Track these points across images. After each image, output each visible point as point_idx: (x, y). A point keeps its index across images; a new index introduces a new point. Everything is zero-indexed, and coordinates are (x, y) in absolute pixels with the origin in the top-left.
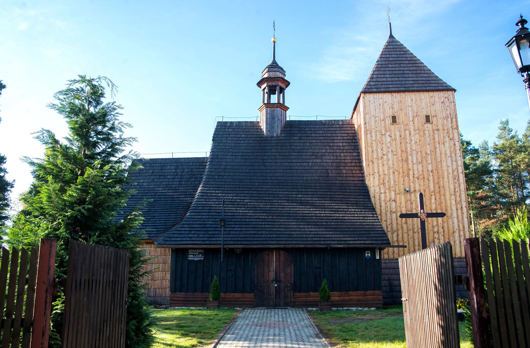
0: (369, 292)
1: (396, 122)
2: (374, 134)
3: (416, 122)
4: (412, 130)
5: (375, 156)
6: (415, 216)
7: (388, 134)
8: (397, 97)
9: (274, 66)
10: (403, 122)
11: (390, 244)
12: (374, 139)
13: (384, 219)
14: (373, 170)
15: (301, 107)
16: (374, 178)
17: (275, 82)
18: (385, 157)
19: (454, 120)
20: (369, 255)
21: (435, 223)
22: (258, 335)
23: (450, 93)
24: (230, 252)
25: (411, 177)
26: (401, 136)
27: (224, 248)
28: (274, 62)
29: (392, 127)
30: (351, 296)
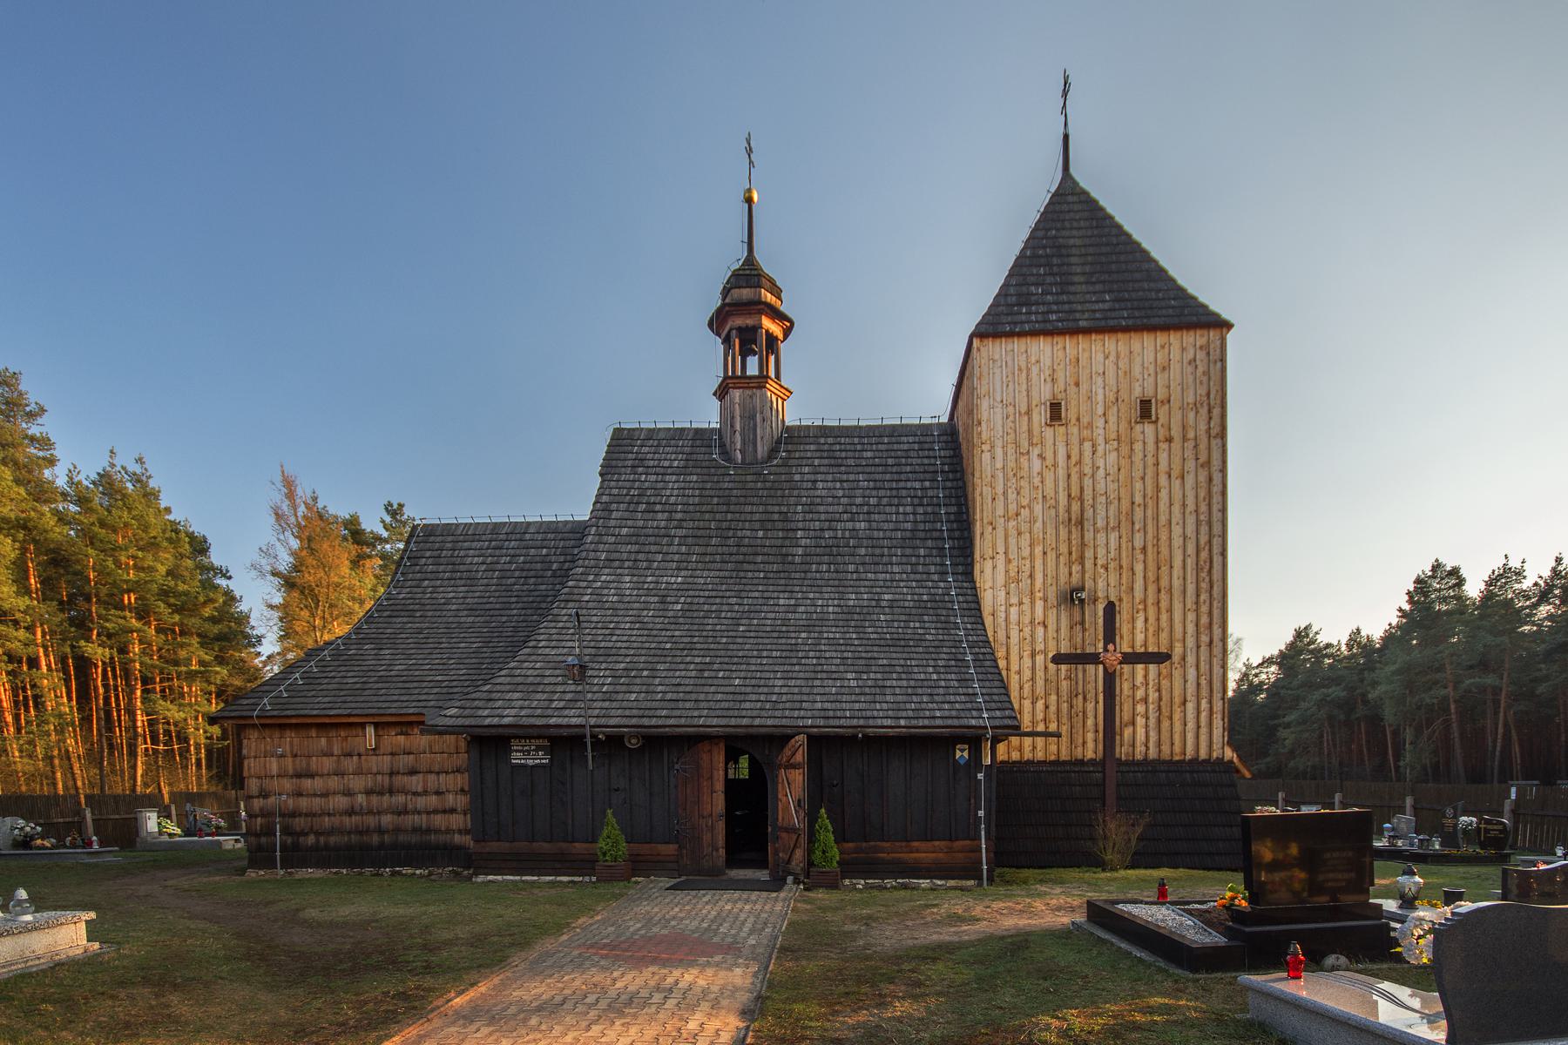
0: (958, 844)
1: (1060, 418)
2: (999, 452)
3: (1112, 419)
4: (1101, 440)
5: (1000, 511)
6: (1094, 659)
7: (1036, 451)
8: (1070, 346)
9: (749, 275)
10: (1078, 420)
11: (1018, 727)
12: (999, 465)
13: (1014, 667)
14: (994, 547)
15: (813, 390)
16: (994, 567)
17: (746, 315)
18: (1025, 513)
19: (1216, 412)
20: (966, 754)
21: (1139, 679)
22: (590, 1006)
23: (1213, 334)
24: (611, 745)
25: (1089, 564)
26: (1069, 457)
27: (592, 736)
28: (750, 261)
29: (1049, 432)
30: (918, 851)
